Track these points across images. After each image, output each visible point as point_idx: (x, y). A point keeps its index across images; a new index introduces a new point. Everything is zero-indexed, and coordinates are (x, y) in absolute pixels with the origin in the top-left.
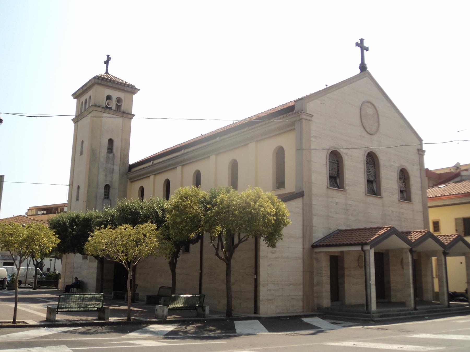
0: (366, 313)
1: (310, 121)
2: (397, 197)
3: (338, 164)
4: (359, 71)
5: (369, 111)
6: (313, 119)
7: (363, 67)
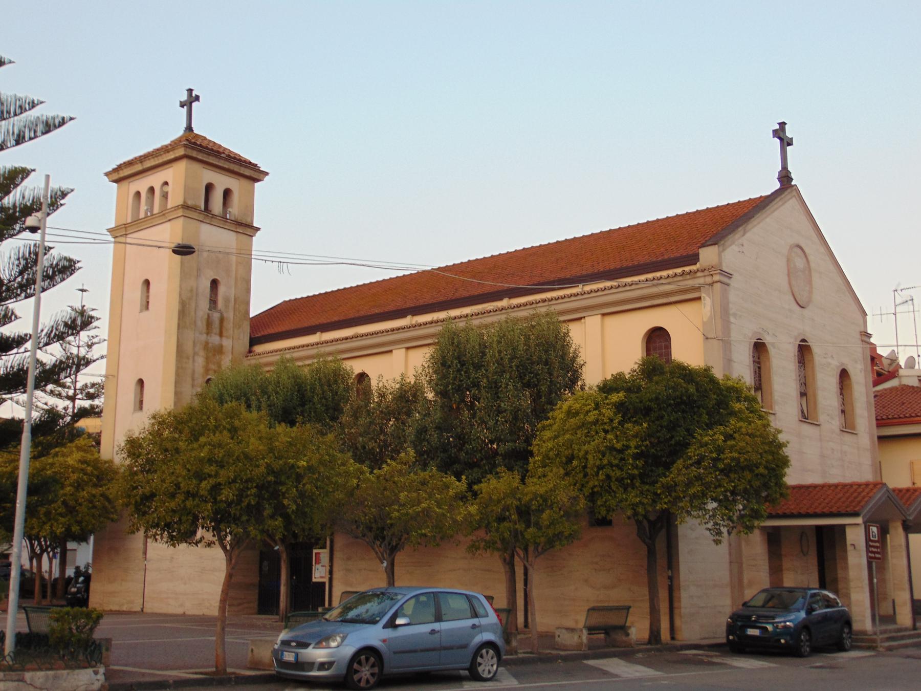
1: (728, 285)
2: (838, 423)
3: (759, 363)
5: (800, 263)
7: (785, 178)
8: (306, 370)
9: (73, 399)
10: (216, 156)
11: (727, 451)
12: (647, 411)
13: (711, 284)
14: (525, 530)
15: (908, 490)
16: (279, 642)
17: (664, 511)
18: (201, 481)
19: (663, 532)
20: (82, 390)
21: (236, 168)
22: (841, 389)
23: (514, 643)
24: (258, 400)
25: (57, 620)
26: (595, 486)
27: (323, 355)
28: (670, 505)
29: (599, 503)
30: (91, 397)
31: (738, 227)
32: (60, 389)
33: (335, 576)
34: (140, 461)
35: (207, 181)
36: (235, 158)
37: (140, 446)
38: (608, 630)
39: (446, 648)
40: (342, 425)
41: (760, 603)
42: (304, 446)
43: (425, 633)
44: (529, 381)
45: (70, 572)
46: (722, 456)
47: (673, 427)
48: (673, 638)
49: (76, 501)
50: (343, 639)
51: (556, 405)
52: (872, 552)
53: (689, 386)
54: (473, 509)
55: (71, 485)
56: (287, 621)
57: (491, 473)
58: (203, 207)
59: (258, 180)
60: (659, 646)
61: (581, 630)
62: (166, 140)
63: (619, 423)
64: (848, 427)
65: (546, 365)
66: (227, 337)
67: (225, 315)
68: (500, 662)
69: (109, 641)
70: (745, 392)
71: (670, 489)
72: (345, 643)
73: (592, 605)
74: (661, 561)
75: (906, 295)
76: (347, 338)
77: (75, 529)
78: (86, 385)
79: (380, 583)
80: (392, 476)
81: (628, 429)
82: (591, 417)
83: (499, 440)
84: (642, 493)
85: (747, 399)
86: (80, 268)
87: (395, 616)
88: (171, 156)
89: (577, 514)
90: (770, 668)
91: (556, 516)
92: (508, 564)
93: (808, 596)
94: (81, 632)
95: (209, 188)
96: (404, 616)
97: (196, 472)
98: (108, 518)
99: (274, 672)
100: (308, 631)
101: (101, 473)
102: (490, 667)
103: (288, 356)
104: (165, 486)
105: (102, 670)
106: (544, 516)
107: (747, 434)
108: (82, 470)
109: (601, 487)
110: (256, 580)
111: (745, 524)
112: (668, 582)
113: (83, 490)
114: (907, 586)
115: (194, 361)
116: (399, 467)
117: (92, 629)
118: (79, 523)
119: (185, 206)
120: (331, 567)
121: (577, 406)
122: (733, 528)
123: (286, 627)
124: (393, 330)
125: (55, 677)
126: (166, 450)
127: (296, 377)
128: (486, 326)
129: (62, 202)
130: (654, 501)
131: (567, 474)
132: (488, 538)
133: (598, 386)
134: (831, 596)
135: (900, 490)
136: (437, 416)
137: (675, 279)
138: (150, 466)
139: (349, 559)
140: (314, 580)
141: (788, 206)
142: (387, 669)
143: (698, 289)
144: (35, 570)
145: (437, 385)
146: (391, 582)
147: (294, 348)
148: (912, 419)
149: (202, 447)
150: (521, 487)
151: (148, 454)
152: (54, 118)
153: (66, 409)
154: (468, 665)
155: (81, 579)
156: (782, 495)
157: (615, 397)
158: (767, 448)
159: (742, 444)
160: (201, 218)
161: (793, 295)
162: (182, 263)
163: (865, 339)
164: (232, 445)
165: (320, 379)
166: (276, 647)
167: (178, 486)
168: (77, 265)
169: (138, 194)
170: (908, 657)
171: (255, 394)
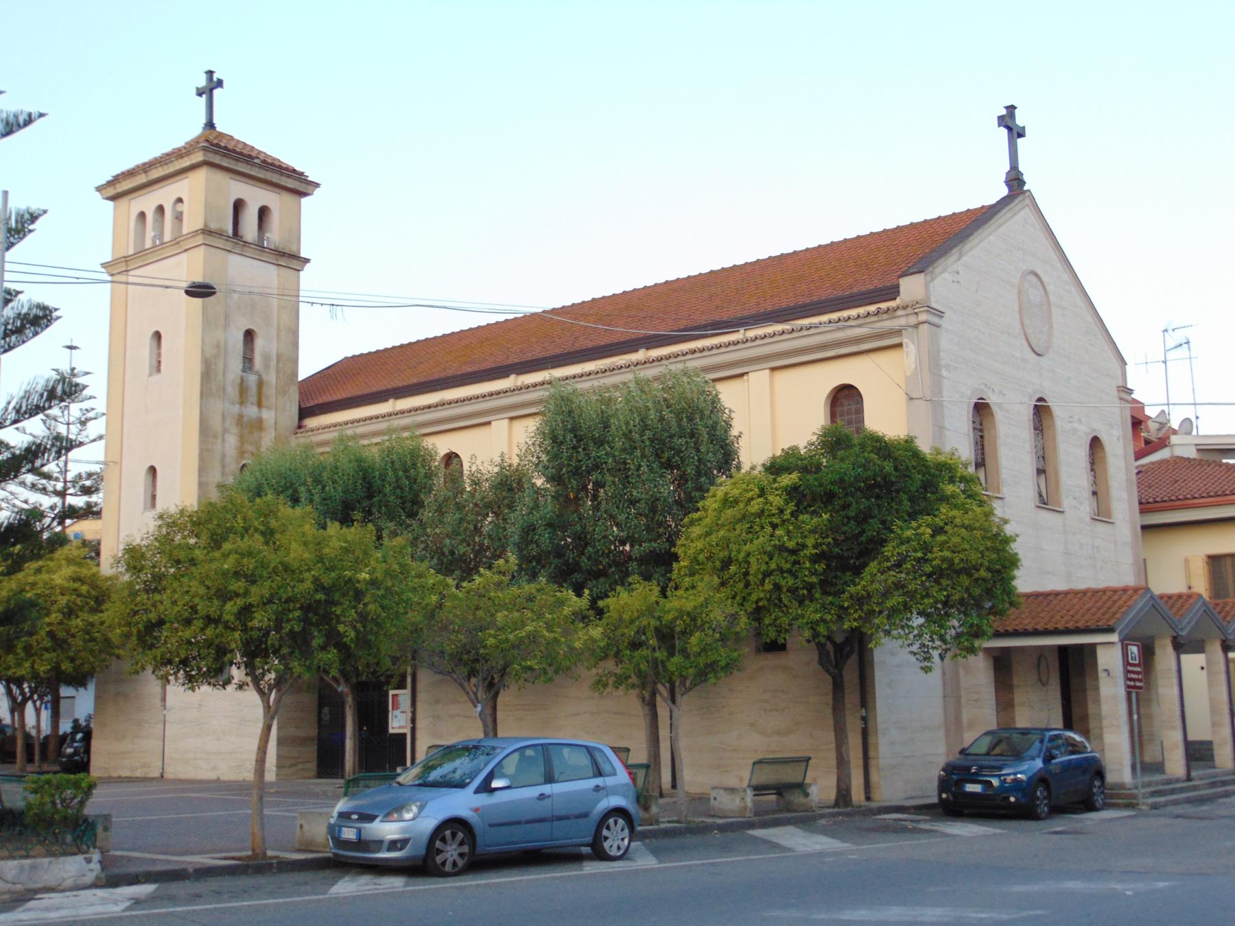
0: (780, 811)
1: (938, 326)
2: (1088, 509)
3: (981, 430)
4: (1004, 191)
6: (944, 322)
7: (1015, 181)
8: (375, 450)
9: (62, 494)
10: (247, 162)
11: (935, 549)
12: (829, 498)
13: (916, 326)
14: (668, 659)
15: (1180, 596)
16: (335, 814)
17: (853, 630)
18: (225, 603)
19: (854, 658)
20: (74, 482)
21: (275, 178)
22: (1092, 463)
23: (654, 809)
24: (309, 491)
25: (35, 792)
26: (760, 599)
27: (394, 430)
28: (861, 623)
29: (767, 621)
30: (87, 491)
31: (951, 248)
32: (44, 481)
33: (419, 725)
34: (142, 576)
35: (235, 194)
36: (272, 164)
37: (143, 556)
38: (780, 789)
39: (560, 818)
40: (422, 525)
41: (983, 750)
42: (366, 553)
43: (532, 799)
44: (669, 460)
45: (65, 727)
46: (929, 556)
47: (863, 518)
48: (868, 799)
49: (68, 632)
50: (421, 808)
51: (708, 491)
52: (1130, 679)
53: (886, 463)
54: (596, 632)
55: (59, 611)
56: (351, 787)
57: (623, 585)
58: (230, 232)
59: (304, 194)
60: (849, 809)
61: (745, 791)
62: (179, 140)
63: (792, 514)
64: (1102, 514)
65: (690, 442)
66: (269, 408)
67: (265, 378)
68: (633, 835)
69: (107, 818)
70: (961, 471)
71: (860, 601)
72: (423, 814)
73: (760, 756)
74: (851, 697)
75: (1179, 337)
76: (429, 407)
77: (66, 666)
78: (80, 476)
79: (474, 732)
80: (488, 591)
81: (803, 522)
82: (755, 507)
83: (633, 541)
84: (823, 606)
85: (964, 479)
86: (58, 318)
87: (490, 777)
88: (186, 162)
89: (738, 638)
90: (995, 835)
91: (709, 640)
92: (648, 704)
93: (1046, 740)
94: (68, 807)
95: (238, 206)
96: (503, 776)
97: (218, 590)
98: (111, 654)
99: (330, 855)
100: (379, 798)
101: (99, 596)
102: (620, 842)
103: (349, 432)
104: (177, 609)
105: (96, 856)
106: (694, 640)
107: (963, 526)
108: (75, 590)
109: (769, 600)
110: (313, 732)
111: (966, 643)
112: (860, 724)
113: (77, 617)
114: (1179, 723)
115: (223, 441)
116: (496, 578)
117: (82, 803)
118: (72, 660)
119: (207, 231)
120: (414, 713)
121: (736, 492)
122: (946, 650)
123: (346, 794)
124: (491, 394)
125: (33, 867)
126: (178, 562)
127: (359, 460)
128: (616, 387)
129: (31, 227)
130: (840, 618)
131: (723, 584)
132: (618, 671)
133: (764, 465)
134: (1078, 738)
135: (1170, 597)
136: (549, 508)
137: (868, 320)
138: (156, 584)
139: (437, 701)
140: (391, 731)
141: (1016, 219)
142: (480, 849)
143: (899, 332)
144: (17, 725)
145: (546, 468)
146: (491, 727)
147: (358, 421)
148: (1195, 501)
149: (226, 556)
150: (662, 601)
151: (154, 567)
152: (16, 116)
153: (52, 508)
154: (589, 839)
155: (79, 736)
156: (1012, 604)
157: (787, 480)
158: (989, 544)
159: (956, 540)
160: (229, 246)
161: (1027, 339)
162: (204, 308)
163: (1126, 396)
164: (267, 552)
165: (393, 463)
166: (332, 821)
167: (194, 609)
168: (55, 314)
169: (142, 215)
170: (1178, 816)
171: (304, 484)
